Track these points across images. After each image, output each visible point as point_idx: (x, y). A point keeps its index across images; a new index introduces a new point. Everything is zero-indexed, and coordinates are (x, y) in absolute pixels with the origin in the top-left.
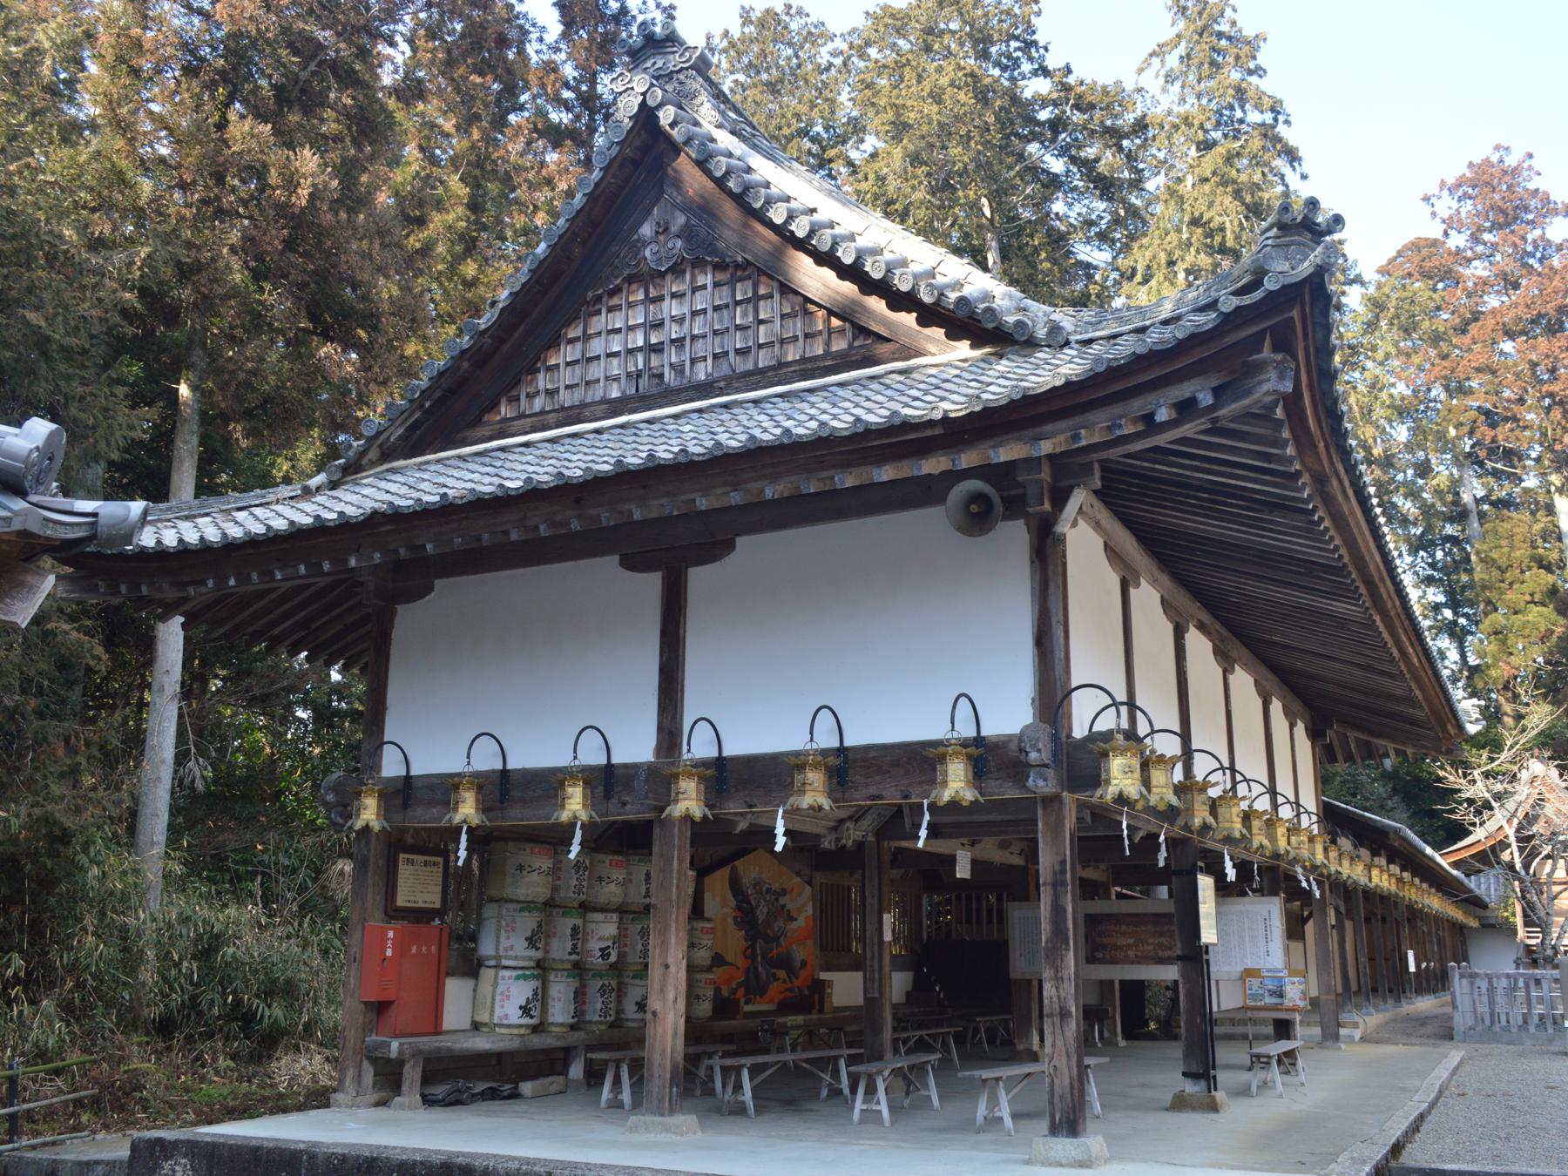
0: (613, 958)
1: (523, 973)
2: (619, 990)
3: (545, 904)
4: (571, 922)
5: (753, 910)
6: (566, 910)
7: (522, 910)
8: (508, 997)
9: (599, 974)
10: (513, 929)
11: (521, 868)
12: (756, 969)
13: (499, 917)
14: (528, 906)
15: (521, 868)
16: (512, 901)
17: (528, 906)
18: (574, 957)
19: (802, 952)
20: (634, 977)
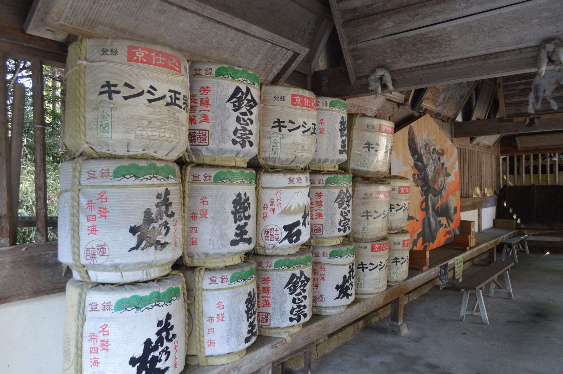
0: (305, 237)
1: (133, 291)
2: (315, 280)
3: (181, 163)
4: (231, 191)
5: (425, 167)
6: (222, 171)
7: (120, 174)
8: (105, 345)
9: (286, 262)
10: (103, 212)
11: (109, 89)
12: (429, 219)
13: (77, 188)
14: (134, 166)
15: (109, 89)
16: (272, 188)
17: (134, 166)
18: (243, 247)
19: (454, 201)
20: (332, 255)
